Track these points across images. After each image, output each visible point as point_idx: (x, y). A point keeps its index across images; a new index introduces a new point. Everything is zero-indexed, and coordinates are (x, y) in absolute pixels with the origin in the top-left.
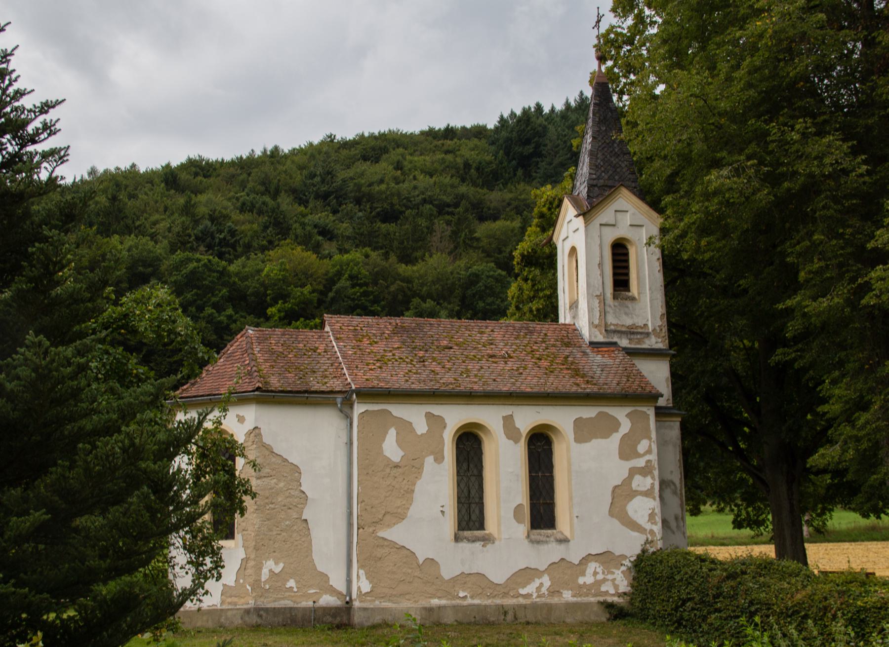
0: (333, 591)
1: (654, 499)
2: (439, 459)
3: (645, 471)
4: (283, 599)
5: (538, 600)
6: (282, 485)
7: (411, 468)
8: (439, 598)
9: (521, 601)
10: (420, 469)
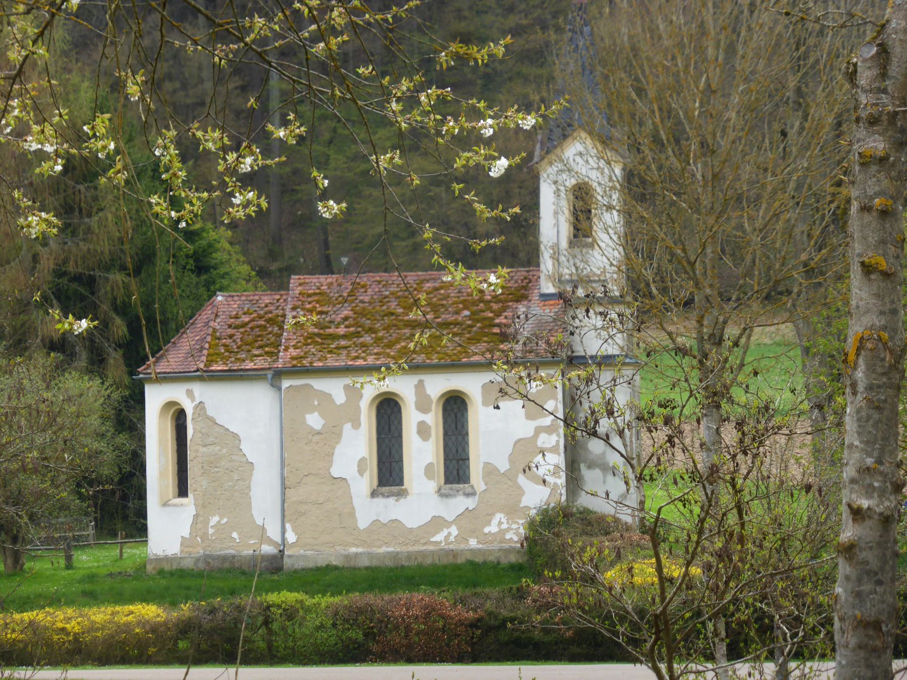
0: (270, 541)
1: (559, 454)
2: (356, 425)
3: (549, 430)
4: (227, 548)
5: (446, 547)
6: (225, 451)
7: (331, 436)
8: (357, 546)
9: (431, 548)
10: (339, 435)
